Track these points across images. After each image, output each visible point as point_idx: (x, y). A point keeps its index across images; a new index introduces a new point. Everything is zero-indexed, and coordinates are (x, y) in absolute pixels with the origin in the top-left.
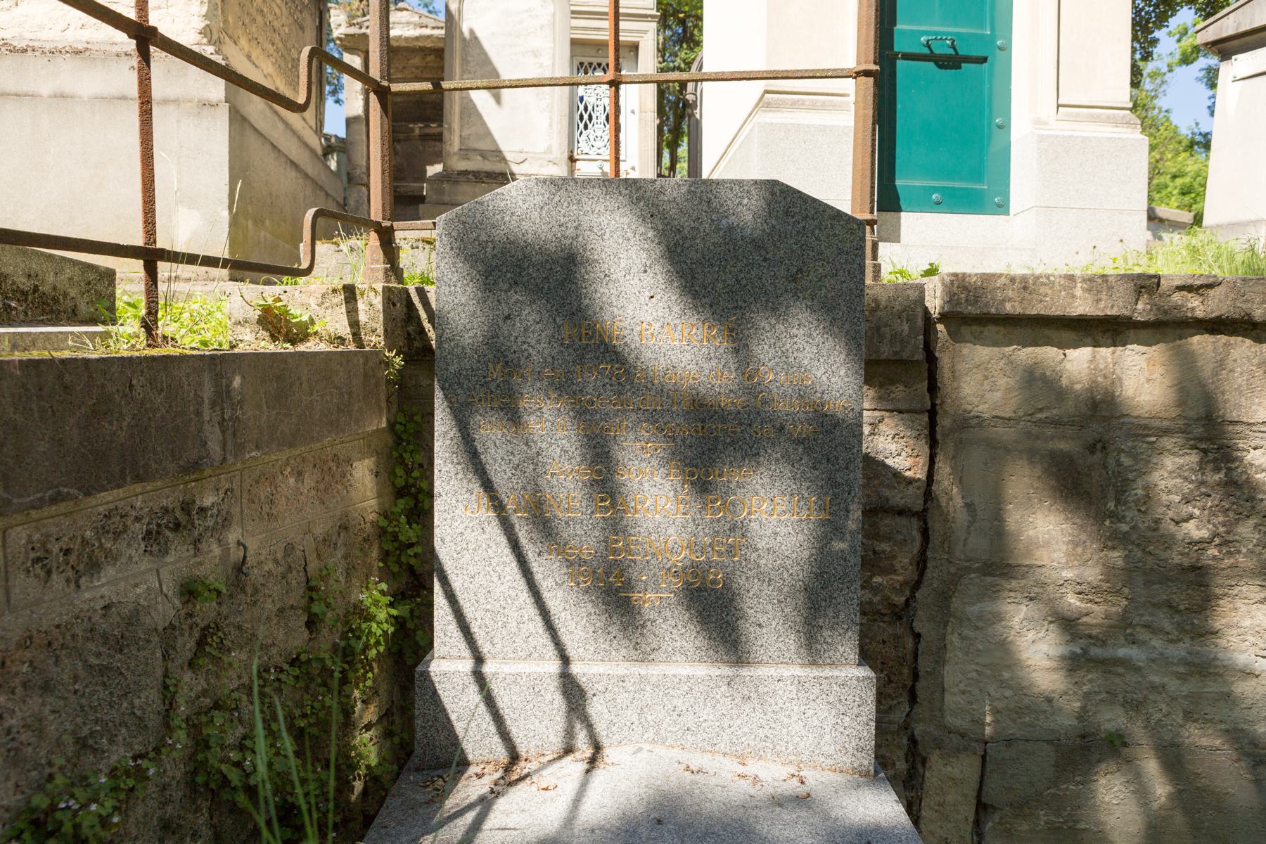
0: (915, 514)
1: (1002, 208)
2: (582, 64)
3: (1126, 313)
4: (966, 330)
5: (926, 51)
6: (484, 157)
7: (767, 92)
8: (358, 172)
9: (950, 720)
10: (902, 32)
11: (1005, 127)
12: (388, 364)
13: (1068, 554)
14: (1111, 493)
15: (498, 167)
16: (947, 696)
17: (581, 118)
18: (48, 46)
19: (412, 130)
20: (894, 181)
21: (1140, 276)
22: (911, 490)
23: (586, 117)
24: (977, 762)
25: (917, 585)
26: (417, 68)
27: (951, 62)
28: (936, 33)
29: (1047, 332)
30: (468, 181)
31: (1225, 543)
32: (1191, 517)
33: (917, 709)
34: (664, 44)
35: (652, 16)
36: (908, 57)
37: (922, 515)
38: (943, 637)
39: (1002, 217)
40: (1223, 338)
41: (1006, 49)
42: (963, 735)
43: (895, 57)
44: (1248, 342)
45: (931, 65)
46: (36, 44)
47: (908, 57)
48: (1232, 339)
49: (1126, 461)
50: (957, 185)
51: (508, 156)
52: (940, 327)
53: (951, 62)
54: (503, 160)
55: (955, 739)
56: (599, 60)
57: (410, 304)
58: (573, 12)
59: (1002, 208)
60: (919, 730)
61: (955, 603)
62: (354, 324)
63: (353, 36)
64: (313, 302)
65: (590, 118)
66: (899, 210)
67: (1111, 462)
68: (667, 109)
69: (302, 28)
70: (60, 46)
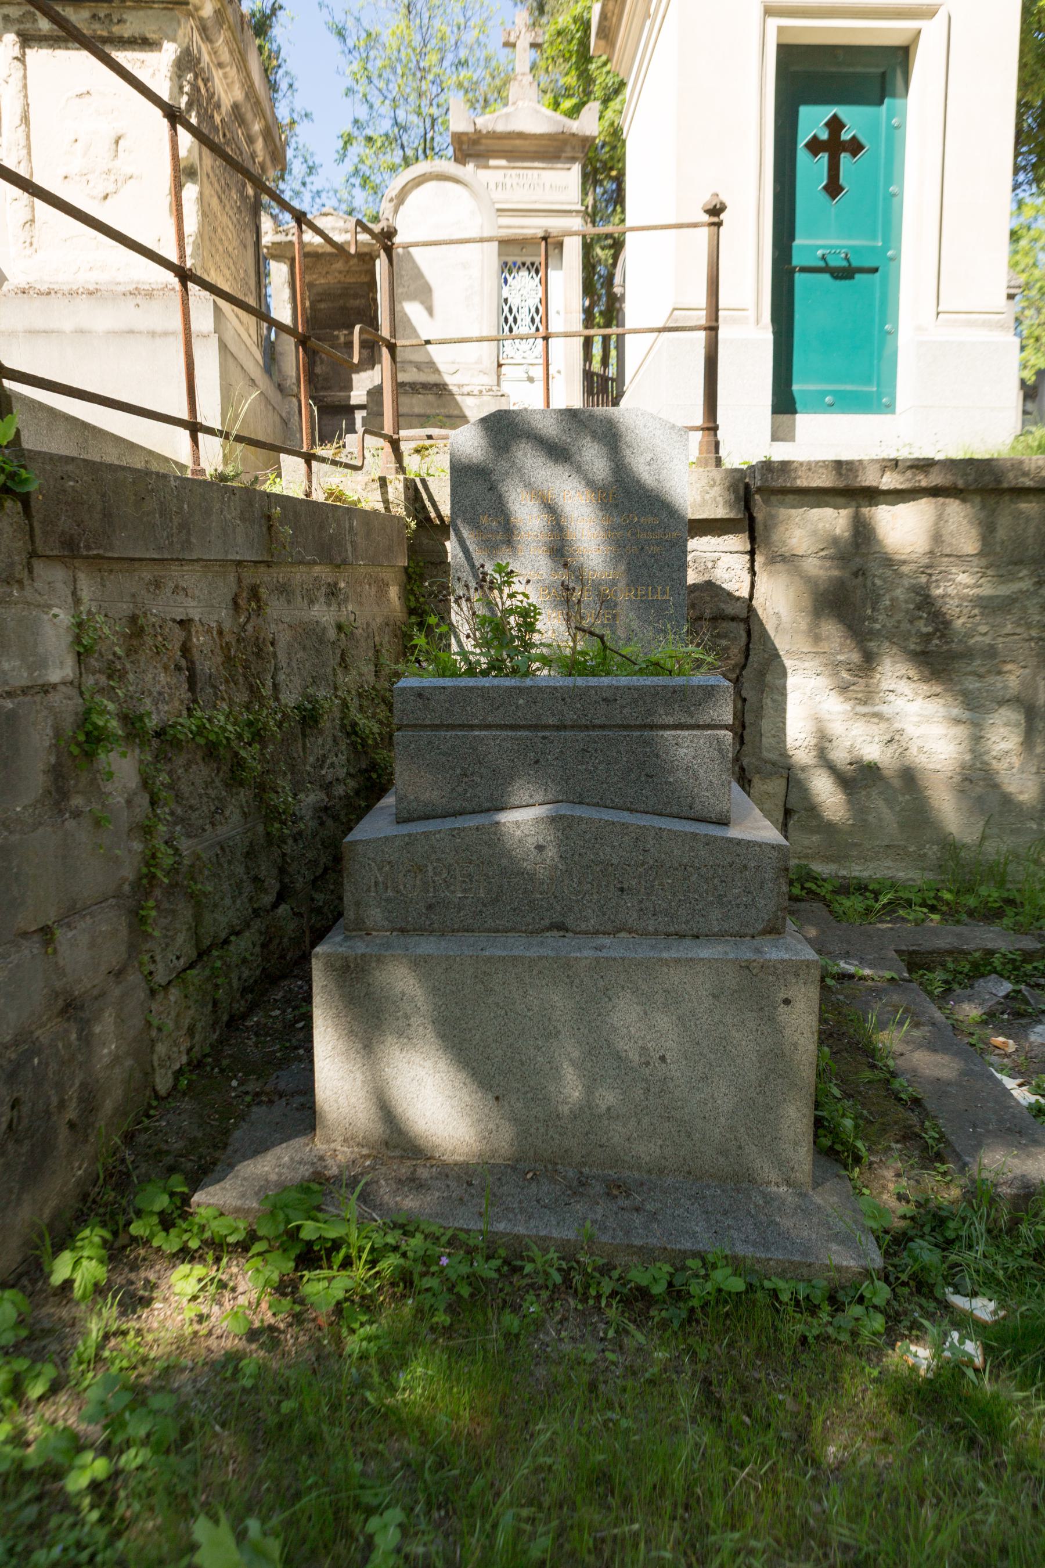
0: (742, 620)
1: (889, 408)
2: (506, 264)
3: (875, 484)
4: (773, 498)
5: (822, 264)
6: (419, 369)
7: (675, 309)
8: (288, 383)
9: (765, 754)
10: (803, 247)
11: (893, 333)
12: (408, 527)
13: (841, 645)
14: (869, 605)
15: (432, 379)
16: (764, 739)
17: (506, 320)
18: (66, 288)
19: (337, 337)
20: (790, 385)
21: (884, 460)
22: (739, 603)
23: (511, 319)
24: (784, 782)
25: (744, 667)
26: (340, 272)
27: (845, 273)
28: (831, 247)
29: (827, 498)
30: (406, 393)
31: (943, 636)
32: (921, 618)
33: (745, 748)
34: (595, 206)
35: (577, 212)
36: (804, 270)
37: (747, 621)
38: (761, 700)
39: (889, 416)
40: (941, 500)
41: (896, 259)
42: (774, 764)
43: (792, 271)
44: (957, 502)
45: (827, 277)
46: (56, 287)
47: (804, 270)
48: (948, 500)
49: (878, 582)
50: (849, 387)
51: (441, 367)
52: (757, 497)
53: (845, 273)
54: (437, 371)
55: (769, 766)
56: (524, 259)
57: (416, 489)
58: (498, 210)
59: (889, 408)
60: (745, 762)
61: (769, 678)
62: (386, 502)
63: (279, 244)
64: (359, 488)
65: (515, 320)
66: (794, 412)
67: (869, 583)
68: (598, 286)
69: (245, 247)
70: (75, 288)
